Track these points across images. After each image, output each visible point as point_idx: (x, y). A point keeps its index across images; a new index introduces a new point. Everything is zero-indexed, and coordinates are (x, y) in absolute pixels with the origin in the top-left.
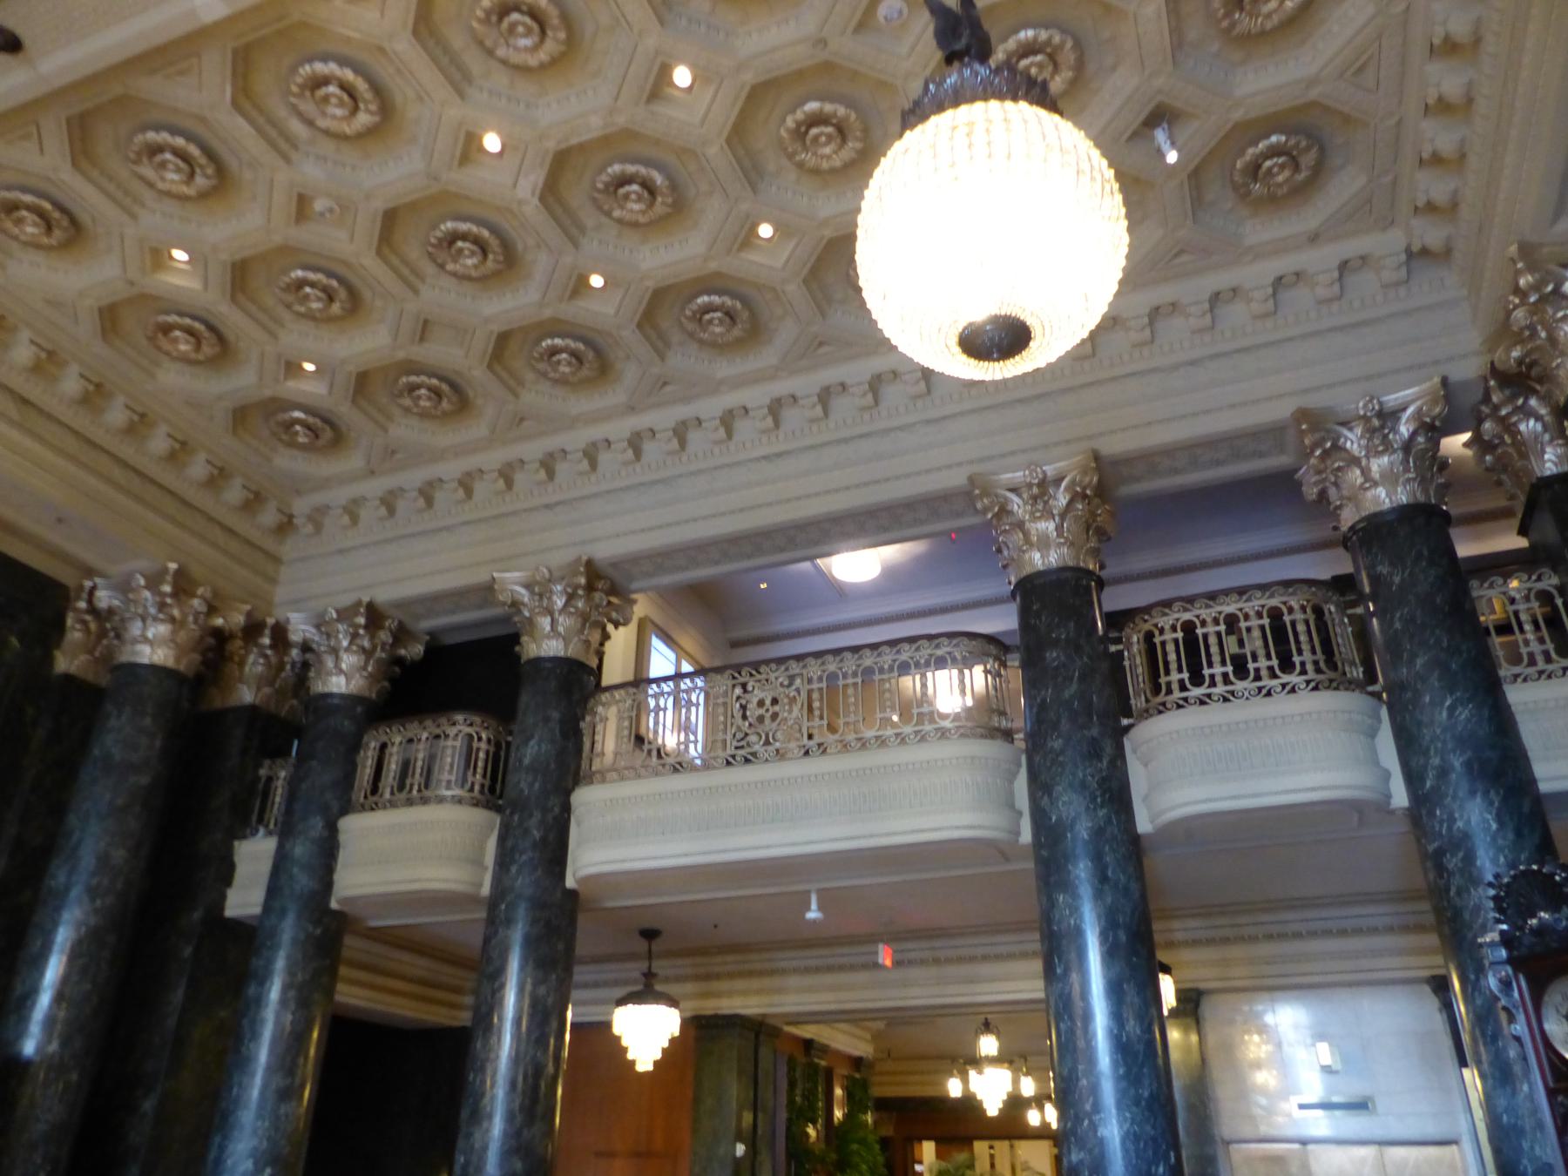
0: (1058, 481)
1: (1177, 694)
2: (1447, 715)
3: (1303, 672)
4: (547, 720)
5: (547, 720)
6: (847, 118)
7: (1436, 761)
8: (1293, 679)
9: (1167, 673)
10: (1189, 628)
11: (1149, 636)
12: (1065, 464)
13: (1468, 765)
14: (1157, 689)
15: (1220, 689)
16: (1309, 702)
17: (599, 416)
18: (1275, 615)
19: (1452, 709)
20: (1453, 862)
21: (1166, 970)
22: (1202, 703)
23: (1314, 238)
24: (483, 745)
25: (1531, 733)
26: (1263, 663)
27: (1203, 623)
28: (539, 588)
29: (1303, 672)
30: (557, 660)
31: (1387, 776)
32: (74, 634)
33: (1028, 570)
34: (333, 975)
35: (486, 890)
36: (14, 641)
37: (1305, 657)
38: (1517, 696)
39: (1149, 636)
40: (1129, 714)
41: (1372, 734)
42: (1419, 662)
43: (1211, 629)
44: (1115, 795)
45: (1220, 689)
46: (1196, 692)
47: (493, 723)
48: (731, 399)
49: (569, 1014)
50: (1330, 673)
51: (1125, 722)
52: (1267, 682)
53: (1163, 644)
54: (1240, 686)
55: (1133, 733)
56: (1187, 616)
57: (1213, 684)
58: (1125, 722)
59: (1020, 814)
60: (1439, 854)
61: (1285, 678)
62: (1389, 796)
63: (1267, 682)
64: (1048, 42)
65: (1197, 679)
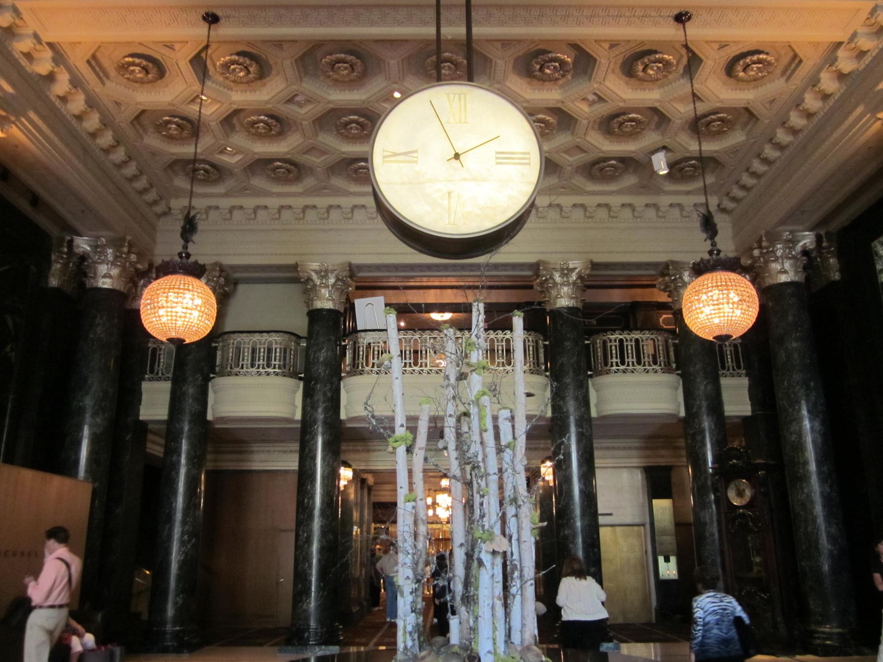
0: (573, 270)
1: (614, 368)
2: (702, 387)
3: (660, 365)
4: (329, 340)
5: (329, 340)
6: (147, 66)
7: (698, 403)
8: (270, 370)
9: (612, 358)
10: (621, 341)
11: (605, 342)
12: (577, 264)
13: (708, 405)
14: (606, 364)
15: (631, 367)
16: (273, 379)
17: (294, 195)
18: (637, 341)
19: (706, 385)
20: (699, 438)
21: (347, 465)
22: (624, 372)
23: (688, 193)
24: (531, 344)
25: (726, 396)
26: (261, 362)
27: (627, 340)
28: (323, 274)
29: (660, 365)
30: (329, 310)
31: (679, 406)
32: (57, 267)
33: (314, 307)
34: (145, 440)
35: (298, 416)
36: (33, 267)
37: (661, 359)
38: (724, 382)
39: (605, 342)
40: (214, 373)
41: (677, 389)
42: (697, 367)
43: (629, 343)
44: (585, 402)
45: (631, 367)
46: (622, 367)
47: (533, 333)
48: (262, 201)
49: (758, 461)
50: (668, 370)
51: (212, 375)
52: (261, 370)
53: (611, 346)
54: (638, 367)
55: (213, 380)
56: (621, 337)
57: (628, 365)
58: (212, 375)
59: (296, 407)
60: (694, 434)
61: (654, 367)
62: (294, 414)
63: (261, 370)
64: (351, 61)
65: (623, 363)
